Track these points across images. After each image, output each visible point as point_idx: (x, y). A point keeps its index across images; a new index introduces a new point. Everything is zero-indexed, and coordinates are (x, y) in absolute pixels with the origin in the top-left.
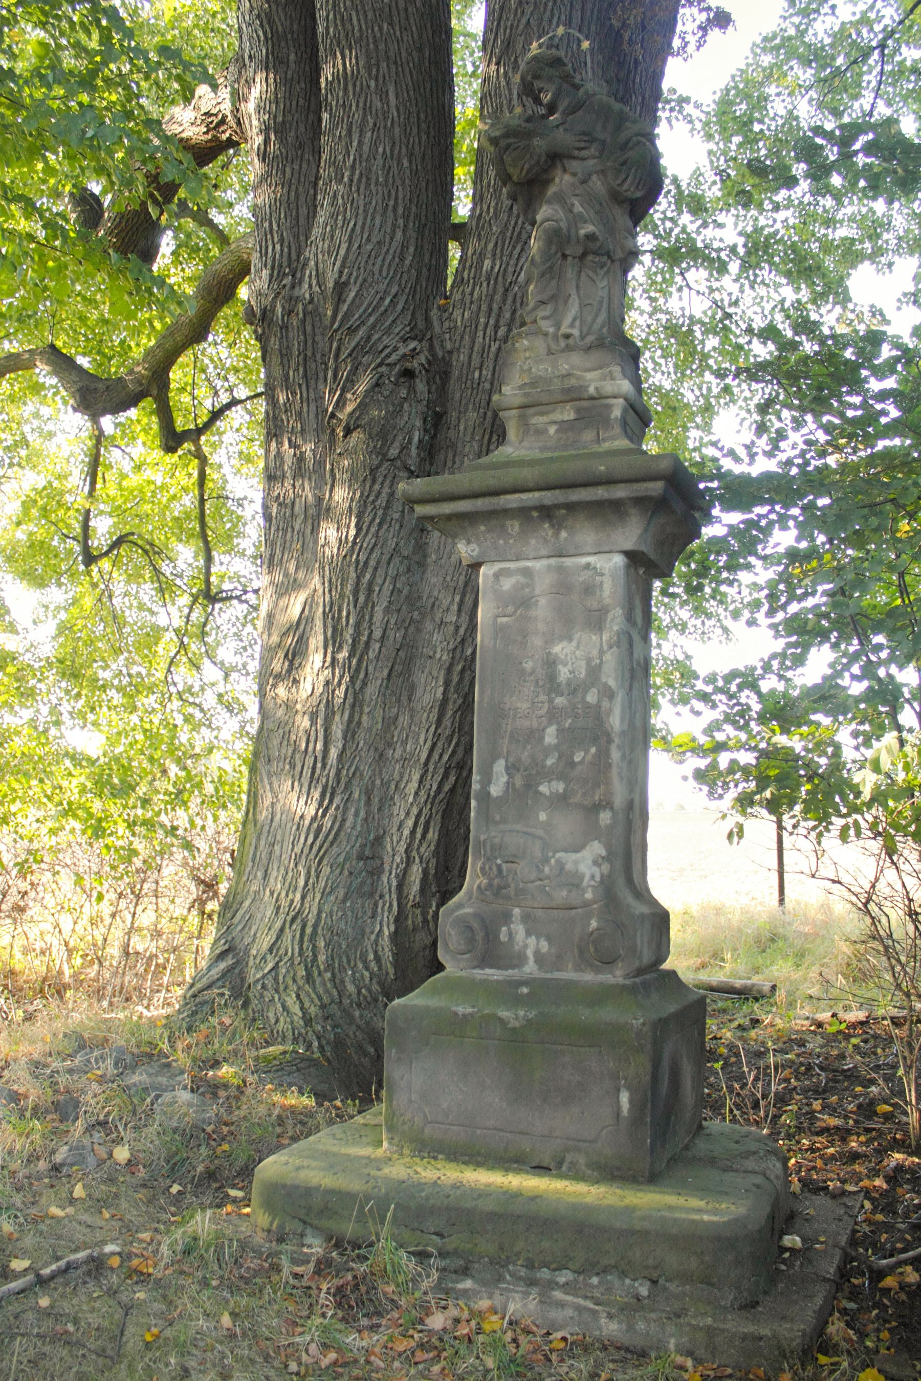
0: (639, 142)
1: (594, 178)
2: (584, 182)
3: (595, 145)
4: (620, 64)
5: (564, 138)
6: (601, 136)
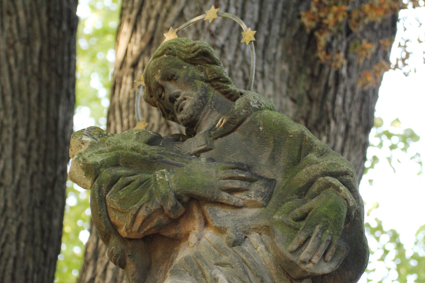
0: (329, 185)
1: (254, 237)
2: (236, 243)
3: (257, 186)
4: (314, 78)
5: (204, 172)
6: (268, 173)
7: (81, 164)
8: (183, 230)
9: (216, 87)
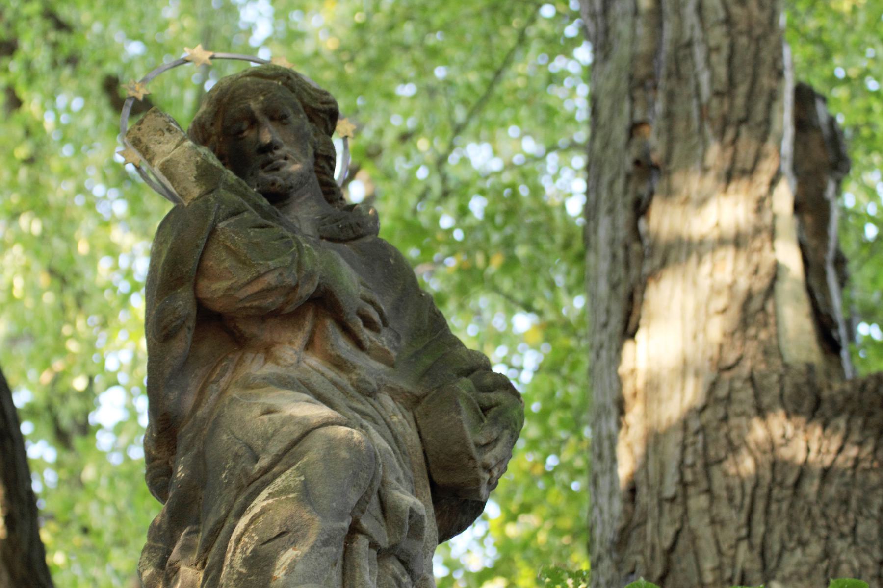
7: (198, 159)
8: (267, 337)
9: (319, 169)
